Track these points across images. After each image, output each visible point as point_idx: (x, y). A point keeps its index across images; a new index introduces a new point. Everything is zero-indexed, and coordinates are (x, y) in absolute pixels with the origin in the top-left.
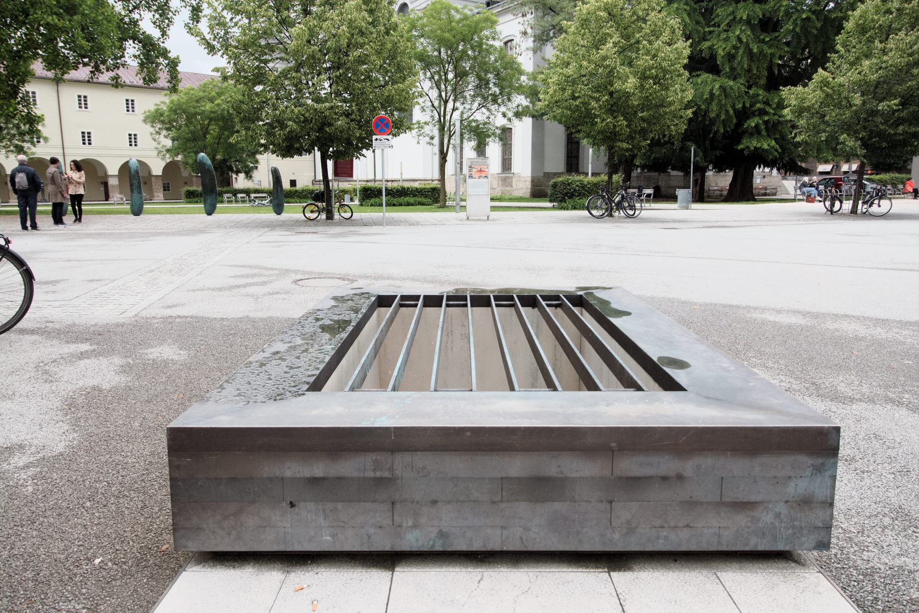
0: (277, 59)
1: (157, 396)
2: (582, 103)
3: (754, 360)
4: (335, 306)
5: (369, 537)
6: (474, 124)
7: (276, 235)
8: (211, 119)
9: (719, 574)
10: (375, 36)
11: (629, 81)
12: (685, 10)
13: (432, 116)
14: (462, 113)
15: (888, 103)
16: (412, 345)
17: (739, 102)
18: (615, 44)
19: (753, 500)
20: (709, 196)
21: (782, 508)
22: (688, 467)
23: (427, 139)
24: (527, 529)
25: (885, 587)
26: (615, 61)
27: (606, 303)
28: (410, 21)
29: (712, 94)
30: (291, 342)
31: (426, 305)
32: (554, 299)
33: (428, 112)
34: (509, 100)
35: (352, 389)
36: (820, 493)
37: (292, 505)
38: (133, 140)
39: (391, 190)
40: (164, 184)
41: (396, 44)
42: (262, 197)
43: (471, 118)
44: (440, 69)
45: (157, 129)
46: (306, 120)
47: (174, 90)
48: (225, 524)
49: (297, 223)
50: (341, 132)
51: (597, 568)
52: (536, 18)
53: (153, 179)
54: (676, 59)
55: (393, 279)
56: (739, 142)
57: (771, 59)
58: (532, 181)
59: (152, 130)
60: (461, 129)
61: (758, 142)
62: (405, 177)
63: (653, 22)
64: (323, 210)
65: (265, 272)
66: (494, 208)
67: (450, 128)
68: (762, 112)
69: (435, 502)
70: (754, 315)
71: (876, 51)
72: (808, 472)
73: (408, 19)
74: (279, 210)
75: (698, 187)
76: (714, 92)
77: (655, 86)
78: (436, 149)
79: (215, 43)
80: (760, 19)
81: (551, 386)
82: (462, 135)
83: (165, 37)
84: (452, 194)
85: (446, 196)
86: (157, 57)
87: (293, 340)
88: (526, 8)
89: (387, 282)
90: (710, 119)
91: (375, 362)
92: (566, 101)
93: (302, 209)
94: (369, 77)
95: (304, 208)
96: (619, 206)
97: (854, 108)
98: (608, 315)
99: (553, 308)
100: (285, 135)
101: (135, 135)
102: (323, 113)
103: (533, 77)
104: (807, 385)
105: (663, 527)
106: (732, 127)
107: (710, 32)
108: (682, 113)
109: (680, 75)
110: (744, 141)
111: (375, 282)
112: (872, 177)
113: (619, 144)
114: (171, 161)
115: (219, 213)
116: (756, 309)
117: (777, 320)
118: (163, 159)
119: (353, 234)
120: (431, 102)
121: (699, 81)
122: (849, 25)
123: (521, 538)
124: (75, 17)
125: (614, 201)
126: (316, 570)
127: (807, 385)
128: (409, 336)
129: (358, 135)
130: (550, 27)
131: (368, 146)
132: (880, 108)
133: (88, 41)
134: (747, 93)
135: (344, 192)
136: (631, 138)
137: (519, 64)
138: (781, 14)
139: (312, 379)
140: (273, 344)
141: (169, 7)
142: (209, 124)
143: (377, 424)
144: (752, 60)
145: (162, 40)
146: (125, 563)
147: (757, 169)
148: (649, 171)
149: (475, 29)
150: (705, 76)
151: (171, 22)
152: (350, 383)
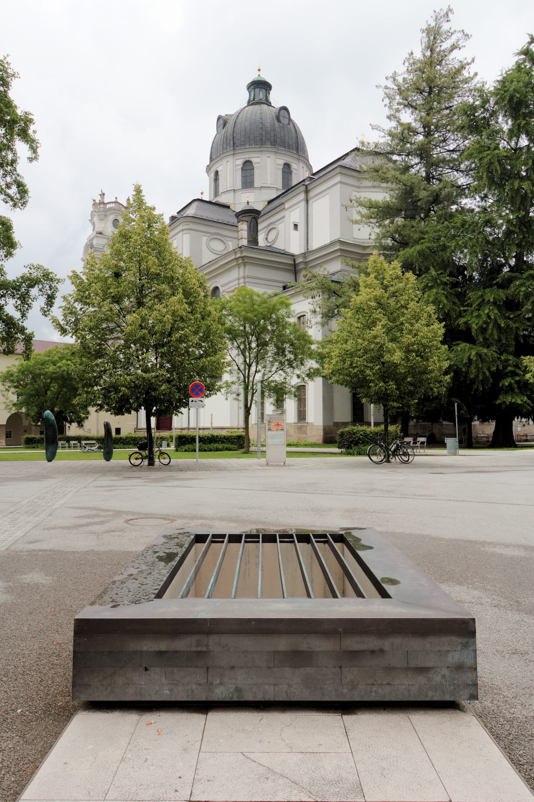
1: (36, 610)
2: (360, 371)
3: (477, 584)
4: (165, 543)
5: (193, 691)
6: (273, 384)
7: (106, 481)
8: (52, 379)
9: (410, 717)
10: (193, 322)
11: (396, 354)
12: (443, 294)
13: (238, 378)
14: (264, 375)
17: (493, 366)
18: (384, 326)
19: (427, 666)
20: (477, 442)
21: (446, 672)
22: (387, 644)
23: (234, 396)
24: (290, 686)
25: (518, 728)
26: (384, 339)
27: (358, 540)
28: (220, 303)
29: (470, 360)
30: (138, 568)
32: (322, 537)
33: (235, 373)
35: (182, 597)
36: (469, 662)
37: (146, 669)
39: (203, 438)
40: (6, 432)
41: (209, 326)
42: (92, 444)
43: (270, 379)
44: (245, 340)
45: (7, 387)
46: (136, 386)
47: (28, 358)
48: (104, 683)
49: (123, 469)
50: (164, 395)
51: (335, 713)
54: (433, 337)
55: (205, 519)
56: (497, 398)
57: (517, 332)
58: (324, 430)
60: (262, 387)
61: (512, 398)
62: (214, 425)
63: (413, 309)
64: (146, 457)
65: (102, 513)
66: (290, 454)
67: (253, 387)
69: (233, 667)
70: (487, 549)
72: (459, 648)
73: (220, 302)
74: (108, 456)
75: (466, 435)
77: (417, 358)
78: (242, 404)
79: (67, 327)
80: (504, 302)
81: (309, 596)
82: (263, 393)
83: (24, 318)
84: (255, 440)
85: (250, 443)
86: (16, 333)
87: (140, 567)
88: (315, 292)
89: (200, 522)
91: (194, 585)
92: (346, 369)
93: (128, 457)
94: (187, 352)
95: (130, 456)
96: (395, 453)
98: (357, 549)
99: (322, 544)
102: (150, 380)
104: (512, 603)
105: (373, 684)
106: (490, 386)
107: (465, 311)
108: (442, 378)
109: (438, 349)
110: (501, 397)
113: (391, 403)
114: (15, 413)
115: (59, 460)
116: (489, 543)
117: (503, 553)
119: (171, 479)
120: (237, 366)
123: (286, 692)
125: (390, 450)
126: (158, 714)
127: (512, 603)
128: (218, 564)
129: (177, 397)
130: (335, 307)
131: (186, 405)
134: (499, 358)
135: (162, 439)
136: (400, 398)
137: (310, 337)
138: (521, 297)
139: (157, 591)
140: (127, 569)
141: (29, 295)
143: (199, 617)
144: (501, 333)
145: (21, 320)
146: (36, 712)
147: (516, 419)
148: (424, 421)
149: (273, 310)
150: (464, 346)
151: (30, 307)
152: (181, 594)
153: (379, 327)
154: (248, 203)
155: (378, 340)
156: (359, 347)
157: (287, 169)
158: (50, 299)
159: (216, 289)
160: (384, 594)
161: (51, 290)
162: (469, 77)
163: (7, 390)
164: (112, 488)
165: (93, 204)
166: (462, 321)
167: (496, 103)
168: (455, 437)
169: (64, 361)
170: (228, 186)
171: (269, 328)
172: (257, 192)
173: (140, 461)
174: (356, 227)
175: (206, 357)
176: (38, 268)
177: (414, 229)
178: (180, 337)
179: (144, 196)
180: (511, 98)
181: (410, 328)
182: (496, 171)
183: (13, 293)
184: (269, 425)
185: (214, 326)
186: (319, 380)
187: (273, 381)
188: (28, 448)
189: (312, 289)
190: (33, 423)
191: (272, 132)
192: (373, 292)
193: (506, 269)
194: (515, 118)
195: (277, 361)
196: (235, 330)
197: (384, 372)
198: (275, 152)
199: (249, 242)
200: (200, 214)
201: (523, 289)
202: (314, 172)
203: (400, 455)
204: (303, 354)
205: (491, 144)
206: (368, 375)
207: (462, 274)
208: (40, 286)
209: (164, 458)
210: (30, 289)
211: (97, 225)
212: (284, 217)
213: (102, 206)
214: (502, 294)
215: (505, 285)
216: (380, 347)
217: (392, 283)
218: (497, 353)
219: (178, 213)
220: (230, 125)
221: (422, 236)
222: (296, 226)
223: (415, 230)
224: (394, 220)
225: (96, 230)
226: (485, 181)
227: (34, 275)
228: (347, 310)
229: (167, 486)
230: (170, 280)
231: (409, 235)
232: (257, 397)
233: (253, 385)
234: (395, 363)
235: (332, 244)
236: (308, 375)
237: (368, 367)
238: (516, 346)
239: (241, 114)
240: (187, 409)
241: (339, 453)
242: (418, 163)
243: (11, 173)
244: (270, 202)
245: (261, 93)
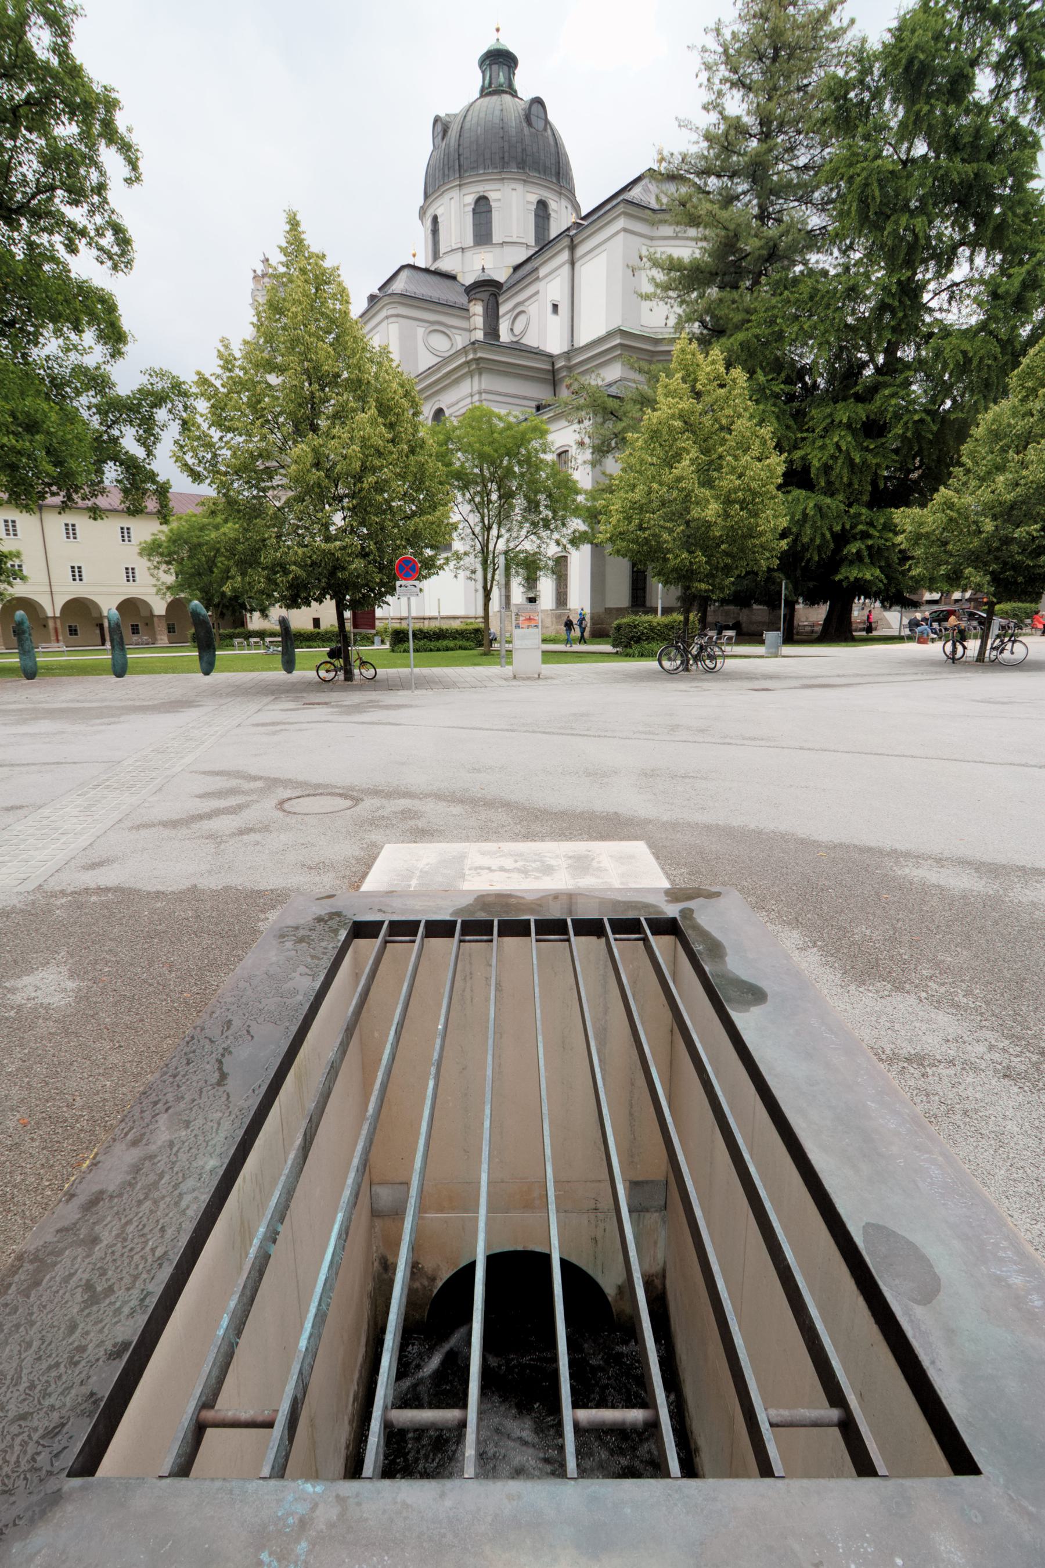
0: (278, 486)
7: (276, 711)
12: (773, 412)
14: (508, 541)
15: (1027, 528)
16: (375, 1128)
18: (693, 461)
23: (468, 573)
28: (444, 432)
29: (805, 515)
34: (564, 525)
38: (131, 575)
43: (518, 549)
45: (155, 563)
46: (313, 564)
52: (595, 423)
53: (155, 619)
56: (836, 571)
59: (149, 564)
61: (859, 571)
62: (443, 613)
68: (865, 535)
71: (1012, 464)
74: (289, 665)
76: (808, 511)
79: (199, 469)
80: (864, 423)
82: (507, 568)
88: (583, 413)
90: (803, 545)
94: (391, 508)
96: (697, 658)
97: (984, 535)
100: (288, 582)
101: (133, 569)
102: (333, 554)
103: (593, 495)
106: (829, 553)
107: (804, 439)
110: (843, 571)
111: (385, 802)
113: (697, 584)
116: (907, 855)
118: (162, 599)
119: (371, 707)
122: (978, 432)
124: (38, 437)
132: (1016, 535)
133: (55, 466)
134: (847, 512)
137: (575, 482)
138: (889, 416)
142: (215, 556)
147: (856, 601)
149: (522, 440)
150: (798, 493)
154: (483, 269)
155: (683, 485)
163: (155, 567)
164: (279, 728)
165: (254, 278)
167: (884, 74)
168: (779, 630)
170: (453, 241)
171: (516, 469)
172: (497, 250)
173: (332, 674)
174: (646, 305)
176: (161, 374)
177: (735, 306)
178: (376, 483)
179: (303, 232)
182: (874, 198)
183: (129, 416)
184: (517, 619)
185: (431, 464)
186: (586, 549)
187: (522, 552)
189: (579, 408)
191: (519, 145)
192: (678, 403)
193: (869, 372)
194: (911, 102)
195: (527, 520)
196: (466, 474)
197: (689, 537)
198: (524, 181)
199: (485, 334)
204: (564, 509)
205: (868, 150)
206: (666, 542)
207: (801, 379)
210: (155, 410)
212: (537, 292)
214: (861, 411)
216: (686, 496)
217: (708, 387)
219: (380, 289)
220: (453, 133)
222: (555, 307)
223: (738, 308)
224: (704, 292)
226: (853, 220)
227: (159, 386)
228: (636, 435)
229: (363, 723)
231: (726, 315)
232: (499, 575)
233: (494, 557)
234: (707, 522)
235: (610, 335)
237: (666, 528)
238: (872, 494)
239: (470, 113)
240: (395, 598)
242: (748, 191)
244: (516, 268)
245: (501, 74)
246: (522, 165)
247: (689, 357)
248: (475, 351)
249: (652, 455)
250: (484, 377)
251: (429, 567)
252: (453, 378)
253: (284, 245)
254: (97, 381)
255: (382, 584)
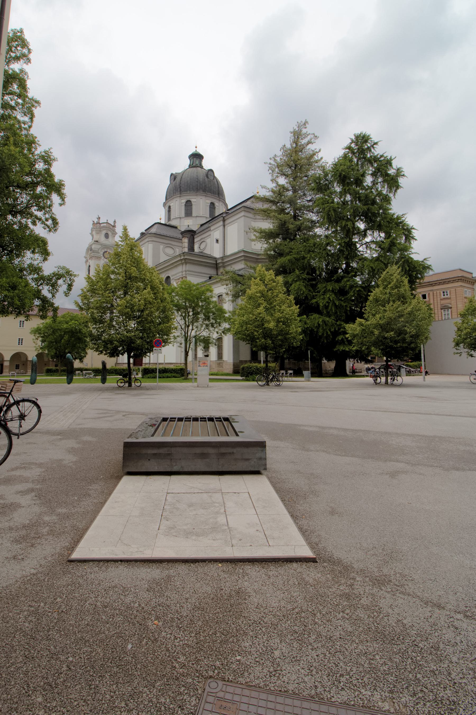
6: (202, 338)
7: (106, 395)
14: (196, 332)
18: (264, 308)
20: (326, 373)
21: (255, 460)
22: (235, 450)
23: (179, 344)
29: (319, 325)
31: (178, 421)
32: (219, 419)
34: (220, 325)
38: (21, 342)
45: (37, 337)
46: (123, 341)
53: (28, 362)
56: (335, 347)
58: (234, 365)
59: (34, 338)
62: (166, 362)
64: (127, 382)
65: (110, 412)
66: (211, 380)
74: (104, 381)
78: (183, 350)
79: (83, 307)
86: (48, 307)
88: (228, 282)
95: (118, 381)
96: (272, 380)
107: (316, 295)
110: (337, 346)
112: (409, 363)
113: (269, 351)
121: (312, 317)
122: (371, 298)
124: (16, 291)
138: (347, 288)
150: (316, 316)
153: (261, 308)
155: (261, 315)
156: (250, 319)
157: (212, 206)
158: (70, 287)
159: (168, 278)
160: (237, 435)
161: (70, 281)
162: (318, 160)
166: (314, 301)
169: (73, 321)
172: (194, 219)
173: (123, 384)
174: (253, 243)
175: (163, 324)
176: (63, 268)
180: (340, 176)
181: (279, 308)
182: (332, 215)
188: (48, 375)
190: (51, 360)
200: (160, 232)
201: (348, 283)
202: (229, 208)
203: (275, 381)
208: (64, 279)
209: (138, 383)
211: (95, 236)
212: (210, 235)
213: (98, 225)
214: (337, 286)
215: (339, 280)
218: (334, 320)
219: (146, 230)
221: (291, 250)
222: (217, 241)
225: (94, 239)
230: (143, 280)
232: (192, 345)
236: (223, 332)
241: (241, 380)
243: (48, 212)
244: (202, 225)
246: (204, 191)
247: (262, 272)
248: (184, 256)
249: (249, 305)
250: (187, 265)
251: (166, 342)
252: (175, 265)
253: (121, 236)
254: (36, 270)
255: (148, 349)
